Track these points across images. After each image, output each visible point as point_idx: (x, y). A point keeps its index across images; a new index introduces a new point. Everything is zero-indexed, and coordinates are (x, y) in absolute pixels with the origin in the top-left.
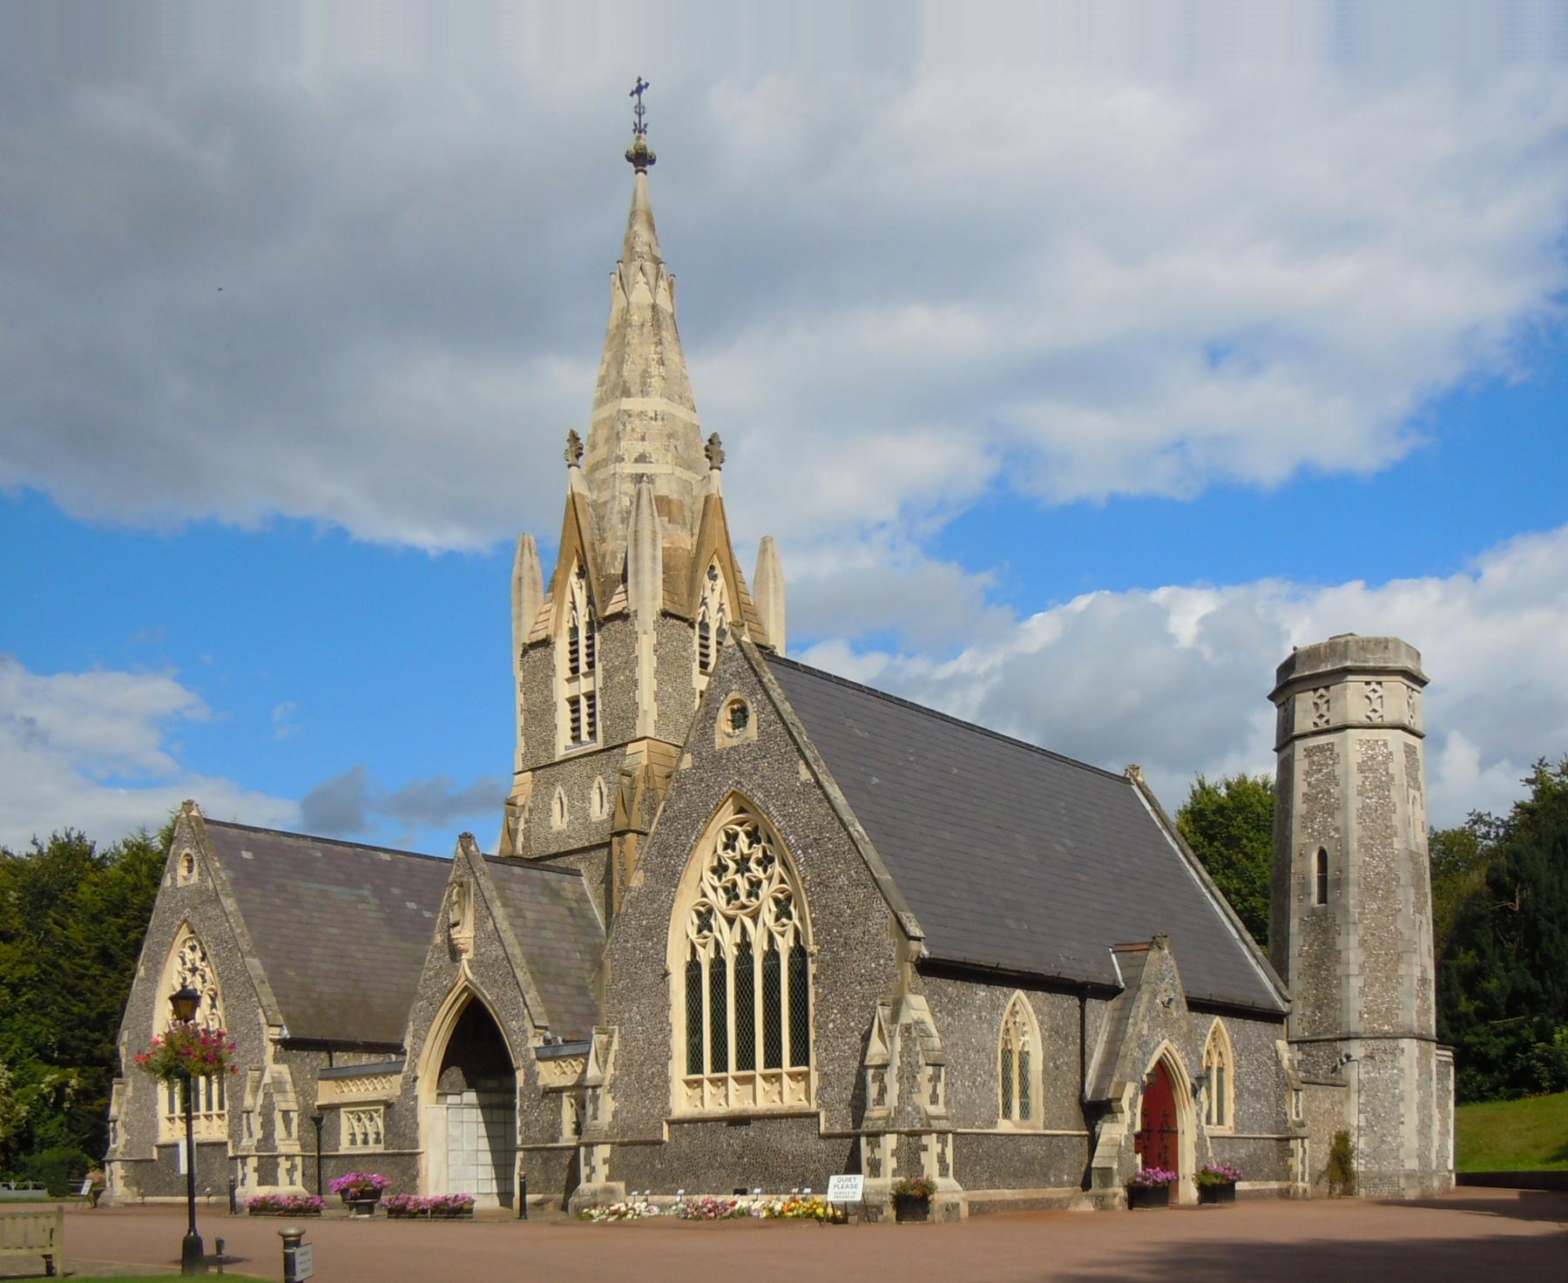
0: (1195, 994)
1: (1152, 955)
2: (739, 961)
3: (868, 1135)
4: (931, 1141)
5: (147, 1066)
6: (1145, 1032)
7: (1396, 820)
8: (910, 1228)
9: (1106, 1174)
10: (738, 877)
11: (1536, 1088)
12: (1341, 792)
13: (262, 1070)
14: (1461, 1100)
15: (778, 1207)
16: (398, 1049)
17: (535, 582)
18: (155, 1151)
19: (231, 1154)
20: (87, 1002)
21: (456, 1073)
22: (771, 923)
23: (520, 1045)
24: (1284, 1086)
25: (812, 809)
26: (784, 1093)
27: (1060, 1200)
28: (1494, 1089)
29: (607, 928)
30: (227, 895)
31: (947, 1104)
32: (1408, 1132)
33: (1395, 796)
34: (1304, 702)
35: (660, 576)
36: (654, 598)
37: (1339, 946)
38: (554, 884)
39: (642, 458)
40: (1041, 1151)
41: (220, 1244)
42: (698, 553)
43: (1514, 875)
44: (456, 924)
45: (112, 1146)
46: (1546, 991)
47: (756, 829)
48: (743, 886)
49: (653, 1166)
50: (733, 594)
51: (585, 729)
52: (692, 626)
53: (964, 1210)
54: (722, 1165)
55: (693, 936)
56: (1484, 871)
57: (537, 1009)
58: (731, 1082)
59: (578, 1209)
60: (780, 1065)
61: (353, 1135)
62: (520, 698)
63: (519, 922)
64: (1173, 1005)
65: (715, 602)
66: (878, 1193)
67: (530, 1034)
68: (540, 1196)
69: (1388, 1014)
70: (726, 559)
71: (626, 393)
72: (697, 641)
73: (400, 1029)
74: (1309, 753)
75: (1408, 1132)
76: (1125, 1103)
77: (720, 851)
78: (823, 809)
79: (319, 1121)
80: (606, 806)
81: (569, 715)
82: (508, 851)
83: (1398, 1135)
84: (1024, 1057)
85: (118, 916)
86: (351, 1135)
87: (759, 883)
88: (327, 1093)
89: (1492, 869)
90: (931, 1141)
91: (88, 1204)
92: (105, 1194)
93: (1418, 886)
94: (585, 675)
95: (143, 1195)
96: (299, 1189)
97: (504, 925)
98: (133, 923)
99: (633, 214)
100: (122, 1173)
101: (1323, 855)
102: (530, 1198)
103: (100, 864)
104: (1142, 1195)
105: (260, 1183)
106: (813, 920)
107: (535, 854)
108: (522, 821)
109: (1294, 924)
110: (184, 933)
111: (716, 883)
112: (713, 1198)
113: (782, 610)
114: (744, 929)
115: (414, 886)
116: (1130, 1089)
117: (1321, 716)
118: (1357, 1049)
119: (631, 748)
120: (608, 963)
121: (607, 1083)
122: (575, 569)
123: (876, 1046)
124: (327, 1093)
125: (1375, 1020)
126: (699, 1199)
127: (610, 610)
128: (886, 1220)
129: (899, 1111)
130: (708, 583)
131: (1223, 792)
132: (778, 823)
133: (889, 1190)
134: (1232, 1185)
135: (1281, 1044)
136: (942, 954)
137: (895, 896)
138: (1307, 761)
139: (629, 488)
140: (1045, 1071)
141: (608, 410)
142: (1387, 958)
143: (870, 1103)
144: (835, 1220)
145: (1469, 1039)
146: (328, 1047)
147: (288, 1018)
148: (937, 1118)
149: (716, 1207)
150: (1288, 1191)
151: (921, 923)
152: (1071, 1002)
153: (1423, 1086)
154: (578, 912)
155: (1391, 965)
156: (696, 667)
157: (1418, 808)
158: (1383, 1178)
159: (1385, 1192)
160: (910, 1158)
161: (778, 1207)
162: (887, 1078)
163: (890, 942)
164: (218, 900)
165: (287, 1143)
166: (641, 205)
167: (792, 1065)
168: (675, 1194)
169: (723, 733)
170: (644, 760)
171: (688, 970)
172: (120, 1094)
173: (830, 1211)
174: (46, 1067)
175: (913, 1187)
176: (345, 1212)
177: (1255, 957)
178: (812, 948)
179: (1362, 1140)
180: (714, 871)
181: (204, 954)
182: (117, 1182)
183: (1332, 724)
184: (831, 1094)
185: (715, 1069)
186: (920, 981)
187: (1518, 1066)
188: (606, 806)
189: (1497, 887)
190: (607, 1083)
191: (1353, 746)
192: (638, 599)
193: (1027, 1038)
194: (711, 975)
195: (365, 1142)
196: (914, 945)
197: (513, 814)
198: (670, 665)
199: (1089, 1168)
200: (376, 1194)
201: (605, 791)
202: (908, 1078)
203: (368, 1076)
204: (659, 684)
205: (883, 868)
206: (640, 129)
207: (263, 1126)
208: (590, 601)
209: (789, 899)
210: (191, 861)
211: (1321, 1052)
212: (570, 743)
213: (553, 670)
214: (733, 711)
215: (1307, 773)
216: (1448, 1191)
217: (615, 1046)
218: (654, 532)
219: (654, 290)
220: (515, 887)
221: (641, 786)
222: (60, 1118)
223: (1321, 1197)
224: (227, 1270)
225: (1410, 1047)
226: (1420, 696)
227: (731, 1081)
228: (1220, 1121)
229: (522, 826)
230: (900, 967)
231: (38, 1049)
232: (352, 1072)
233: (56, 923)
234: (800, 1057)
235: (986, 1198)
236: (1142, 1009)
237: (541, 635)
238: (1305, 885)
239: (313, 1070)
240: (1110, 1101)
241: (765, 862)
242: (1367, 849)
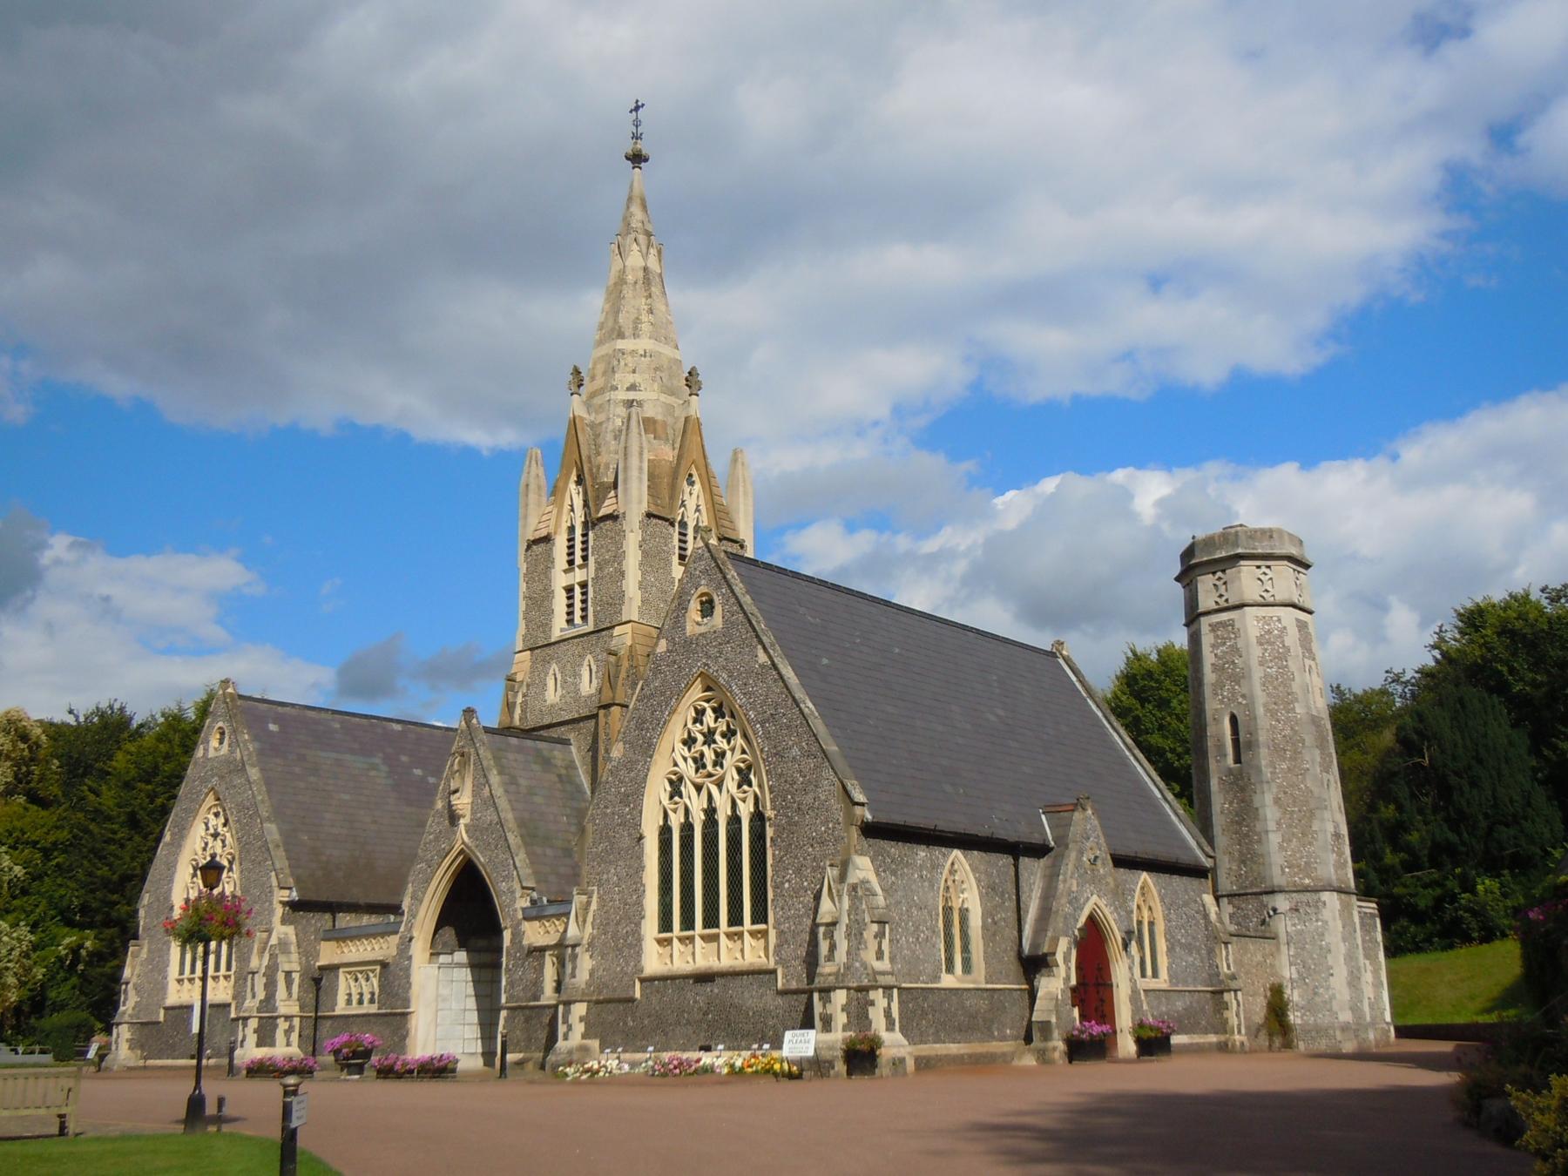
0: (1123, 851)
1: (1077, 815)
3: (821, 991)
4: (877, 996)
5: (171, 929)
6: (1074, 888)
7: (1295, 687)
8: (860, 1083)
9: (1046, 1027)
10: (705, 749)
11: (1467, 939)
13: (269, 931)
14: (1392, 951)
15: (739, 1063)
16: (396, 909)
17: (539, 488)
18: (162, 1012)
19: (233, 1015)
20: (110, 865)
21: (449, 933)
22: (734, 790)
23: (509, 906)
24: (1215, 939)
25: (769, 688)
26: (741, 950)
27: (1004, 1054)
28: (1428, 940)
29: (593, 792)
30: (253, 766)
31: (892, 960)
32: (1339, 981)
33: (1293, 665)
34: (1205, 583)
35: (646, 483)
36: (640, 502)
37: (1256, 804)
38: (545, 753)
39: (632, 388)
40: (983, 1005)
41: (221, 1102)
42: (679, 463)
43: (1419, 733)
44: (456, 791)
45: (122, 1008)
46: (1464, 844)
47: (721, 705)
48: (709, 756)
49: (625, 1023)
51: (578, 613)
52: (672, 524)
53: (910, 1064)
54: (689, 1023)
55: (666, 802)
56: (1393, 729)
57: (526, 871)
58: (698, 940)
59: (555, 1067)
60: (741, 924)
61: (350, 995)
62: (523, 586)
63: (513, 788)
64: (1099, 862)
65: (693, 504)
66: (831, 1048)
67: (518, 894)
68: (521, 1055)
69: (1307, 869)
71: (621, 335)
72: (676, 537)
73: (399, 890)
74: (1214, 628)
75: (1339, 981)
76: (1059, 957)
77: (690, 725)
78: (778, 688)
79: (319, 981)
80: (595, 681)
81: (565, 601)
82: (507, 723)
83: (1328, 988)
84: (964, 913)
85: (148, 782)
86: (351, 996)
87: (723, 754)
88: (329, 953)
89: (1400, 729)
91: (92, 1069)
92: (109, 1057)
93: (1322, 746)
94: (580, 567)
95: (145, 1058)
96: (295, 1051)
97: (498, 791)
98: (159, 789)
99: (630, 199)
100: (127, 1035)
101: (1234, 720)
102: (510, 1057)
103: (138, 734)
104: (1079, 1049)
105: (259, 1045)
106: (770, 788)
107: (530, 724)
108: (520, 695)
110: (210, 800)
111: (687, 754)
112: (679, 1054)
113: (751, 509)
115: (419, 753)
116: (1063, 945)
118: (1282, 903)
119: (617, 631)
120: (590, 828)
121: (585, 942)
122: (574, 477)
123: (826, 905)
124: (329, 953)
125: (1296, 874)
126: (666, 1056)
128: (837, 1075)
129: (848, 967)
130: (687, 489)
131: (1154, 657)
132: (739, 701)
133: (840, 1045)
134: (1167, 1038)
135: (1208, 899)
136: (884, 818)
137: (841, 765)
139: (622, 411)
140: (984, 927)
141: (605, 349)
142: (1302, 816)
143: (822, 960)
144: (790, 1076)
145: (1396, 890)
146: (332, 908)
147: (298, 881)
148: (883, 973)
149: (681, 1064)
151: (865, 790)
152: (1005, 861)
153: (1348, 937)
155: (1306, 822)
156: (675, 559)
157: (1314, 676)
158: (1320, 1031)
159: (1322, 1045)
160: (859, 1013)
161: (739, 1063)
162: (836, 937)
163: (836, 805)
164: (243, 769)
165: (287, 1004)
166: (636, 191)
167: (753, 923)
168: (645, 1051)
171: (660, 834)
172: (135, 956)
173: (786, 1067)
174: (66, 930)
175: (862, 1042)
176: (336, 1074)
177: (1176, 814)
179: (1296, 993)
180: (685, 743)
182: (123, 1046)
183: (1231, 602)
184: (787, 952)
185: (731, 923)
186: (865, 843)
187: (1447, 917)
188: (595, 681)
189: (1407, 745)
190: (585, 942)
191: (1251, 622)
192: (627, 502)
194: (681, 837)
195: (360, 1002)
196: (858, 810)
197: (512, 689)
198: (652, 558)
199: (1030, 1022)
200: (367, 1054)
201: (594, 668)
202: (855, 934)
203: (368, 936)
205: (830, 740)
206: (636, 137)
207: (266, 986)
208: (586, 505)
209: (749, 768)
210: (222, 734)
211: (1250, 906)
212: (565, 625)
214: (702, 603)
215: (1213, 646)
216: (1388, 1044)
217: (594, 906)
218: (641, 447)
219: (645, 256)
220: (511, 756)
221: (625, 664)
222: (74, 980)
223: (1262, 1051)
224: (226, 1128)
225: (1331, 899)
226: (1305, 577)
227: (698, 939)
228: (1155, 974)
229: (519, 699)
230: (847, 831)
231: (61, 913)
232: (354, 933)
233: (91, 790)
234: (760, 915)
235: (933, 1053)
236: (1070, 866)
237: (543, 533)
238: (1220, 747)
239: (317, 931)
240: (1045, 955)
241: (729, 734)
242: (1273, 714)
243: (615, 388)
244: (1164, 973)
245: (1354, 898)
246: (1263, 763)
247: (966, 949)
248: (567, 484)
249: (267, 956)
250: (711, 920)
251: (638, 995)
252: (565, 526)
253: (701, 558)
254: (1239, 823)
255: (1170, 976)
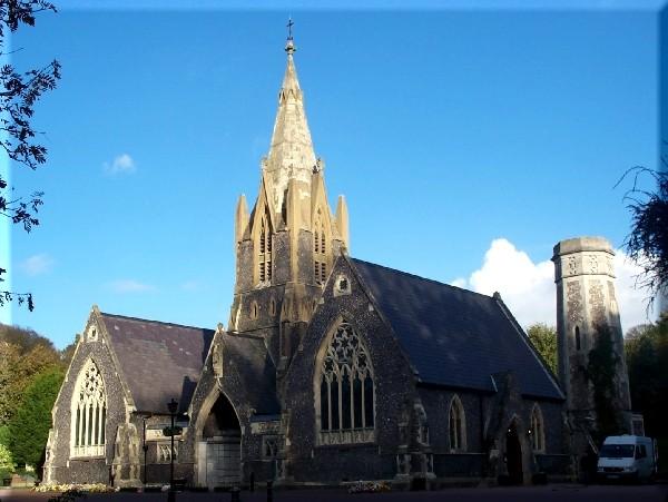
22: (357, 367)
74: (569, 284)
104: (503, 481)
114: (345, 369)
135: (564, 414)
181: (98, 372)
196: (415, 378)
228: (540, 448)
244: (543, 448)
247: (459, 439)
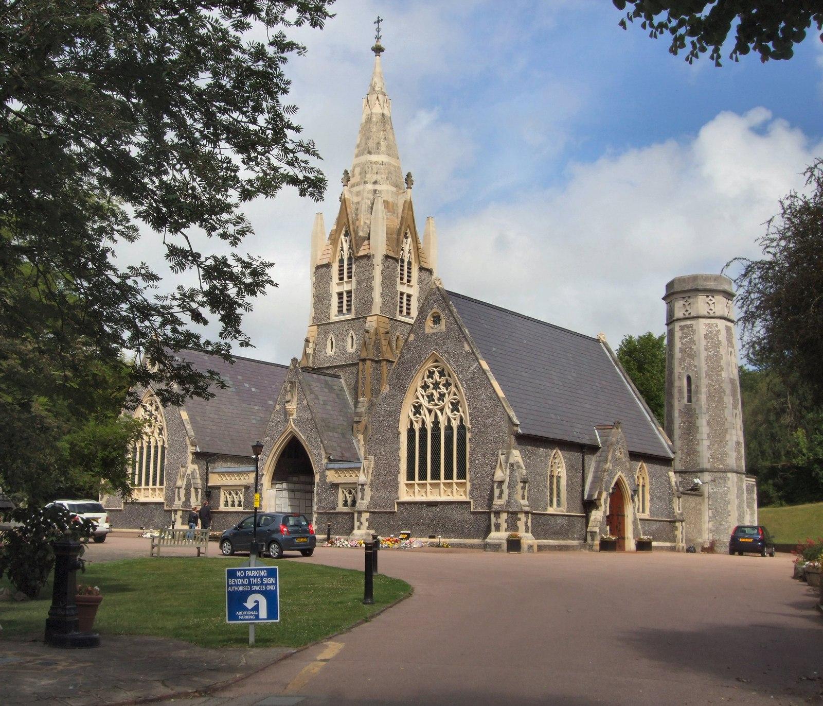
2: (433, 429)
4: (522, 516)
6: (611, 468)
7: (723, 363)
9: (593, 534)
10: (434, 391)
12: (697, 348)
14: (761, 504)
22: (449, 414)
33: (723, 351)
37: (698, 425)
47: (443, 370)
50: (415, 245)
51: (345, 307)
52: (397, 261)
53: (535, 548)
58: (442, 486)
61: (227, 502)
69: (722, 460)
70: (413, 230)
72: (399, 267)
74: (682, 328)
76: (602, 501)
88: (214, 480)
90: (522, 516)
93: (734, 394)
101: (689, 378)
104: (606, 546)
109: (676, 414)
117: (687, 311)
122: (343, 232)
127: (361, 253)
135: (671, 474)
138: (680, 332)
140: (568, 485)
142: (719, 436)
150: (675, 547)
152: (578, 455)
153: (740, 496)
154: (340, 394)
156: (398, 280)
163: (505, 426)
169: (429, 327)
170: (374, 324)
178: (468, 425)
180: (422, 387)
183: (692, 315)
184: (475, 493)
190: (369, 483)
191: (702, 326)
193: (560, 470)
195: (233, 505)
196: (515, 428)
199: (587, 532)
201: (355, 338)
202: (512, 486)
204: (383, 289)
206: (378, 38)
207: (185, 495)
208: (350, 248)
213: (331, 278)
219: (382, 108)
228: (643, 511)
234: (461, 475)
237: (325, 262)
243: (366, 183)
245: (744, 476)
246: (703, 403)
247: (558, 495)
248: (339, 236)
249: (185, 479)
250: (436, 476)
251: (396, 510)
252: (337, 259)
253: (434, 294)
254: (688, 434)
255: (651, 512)
